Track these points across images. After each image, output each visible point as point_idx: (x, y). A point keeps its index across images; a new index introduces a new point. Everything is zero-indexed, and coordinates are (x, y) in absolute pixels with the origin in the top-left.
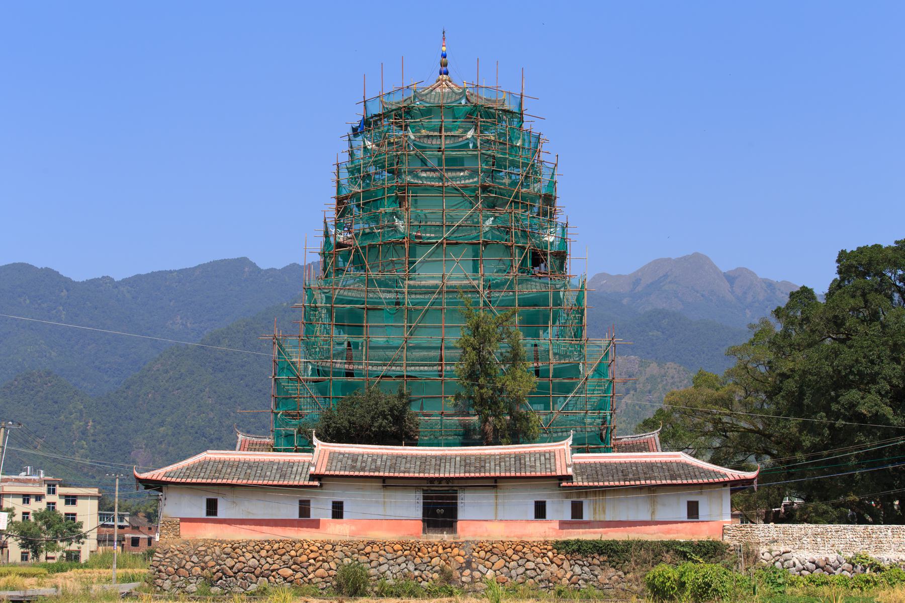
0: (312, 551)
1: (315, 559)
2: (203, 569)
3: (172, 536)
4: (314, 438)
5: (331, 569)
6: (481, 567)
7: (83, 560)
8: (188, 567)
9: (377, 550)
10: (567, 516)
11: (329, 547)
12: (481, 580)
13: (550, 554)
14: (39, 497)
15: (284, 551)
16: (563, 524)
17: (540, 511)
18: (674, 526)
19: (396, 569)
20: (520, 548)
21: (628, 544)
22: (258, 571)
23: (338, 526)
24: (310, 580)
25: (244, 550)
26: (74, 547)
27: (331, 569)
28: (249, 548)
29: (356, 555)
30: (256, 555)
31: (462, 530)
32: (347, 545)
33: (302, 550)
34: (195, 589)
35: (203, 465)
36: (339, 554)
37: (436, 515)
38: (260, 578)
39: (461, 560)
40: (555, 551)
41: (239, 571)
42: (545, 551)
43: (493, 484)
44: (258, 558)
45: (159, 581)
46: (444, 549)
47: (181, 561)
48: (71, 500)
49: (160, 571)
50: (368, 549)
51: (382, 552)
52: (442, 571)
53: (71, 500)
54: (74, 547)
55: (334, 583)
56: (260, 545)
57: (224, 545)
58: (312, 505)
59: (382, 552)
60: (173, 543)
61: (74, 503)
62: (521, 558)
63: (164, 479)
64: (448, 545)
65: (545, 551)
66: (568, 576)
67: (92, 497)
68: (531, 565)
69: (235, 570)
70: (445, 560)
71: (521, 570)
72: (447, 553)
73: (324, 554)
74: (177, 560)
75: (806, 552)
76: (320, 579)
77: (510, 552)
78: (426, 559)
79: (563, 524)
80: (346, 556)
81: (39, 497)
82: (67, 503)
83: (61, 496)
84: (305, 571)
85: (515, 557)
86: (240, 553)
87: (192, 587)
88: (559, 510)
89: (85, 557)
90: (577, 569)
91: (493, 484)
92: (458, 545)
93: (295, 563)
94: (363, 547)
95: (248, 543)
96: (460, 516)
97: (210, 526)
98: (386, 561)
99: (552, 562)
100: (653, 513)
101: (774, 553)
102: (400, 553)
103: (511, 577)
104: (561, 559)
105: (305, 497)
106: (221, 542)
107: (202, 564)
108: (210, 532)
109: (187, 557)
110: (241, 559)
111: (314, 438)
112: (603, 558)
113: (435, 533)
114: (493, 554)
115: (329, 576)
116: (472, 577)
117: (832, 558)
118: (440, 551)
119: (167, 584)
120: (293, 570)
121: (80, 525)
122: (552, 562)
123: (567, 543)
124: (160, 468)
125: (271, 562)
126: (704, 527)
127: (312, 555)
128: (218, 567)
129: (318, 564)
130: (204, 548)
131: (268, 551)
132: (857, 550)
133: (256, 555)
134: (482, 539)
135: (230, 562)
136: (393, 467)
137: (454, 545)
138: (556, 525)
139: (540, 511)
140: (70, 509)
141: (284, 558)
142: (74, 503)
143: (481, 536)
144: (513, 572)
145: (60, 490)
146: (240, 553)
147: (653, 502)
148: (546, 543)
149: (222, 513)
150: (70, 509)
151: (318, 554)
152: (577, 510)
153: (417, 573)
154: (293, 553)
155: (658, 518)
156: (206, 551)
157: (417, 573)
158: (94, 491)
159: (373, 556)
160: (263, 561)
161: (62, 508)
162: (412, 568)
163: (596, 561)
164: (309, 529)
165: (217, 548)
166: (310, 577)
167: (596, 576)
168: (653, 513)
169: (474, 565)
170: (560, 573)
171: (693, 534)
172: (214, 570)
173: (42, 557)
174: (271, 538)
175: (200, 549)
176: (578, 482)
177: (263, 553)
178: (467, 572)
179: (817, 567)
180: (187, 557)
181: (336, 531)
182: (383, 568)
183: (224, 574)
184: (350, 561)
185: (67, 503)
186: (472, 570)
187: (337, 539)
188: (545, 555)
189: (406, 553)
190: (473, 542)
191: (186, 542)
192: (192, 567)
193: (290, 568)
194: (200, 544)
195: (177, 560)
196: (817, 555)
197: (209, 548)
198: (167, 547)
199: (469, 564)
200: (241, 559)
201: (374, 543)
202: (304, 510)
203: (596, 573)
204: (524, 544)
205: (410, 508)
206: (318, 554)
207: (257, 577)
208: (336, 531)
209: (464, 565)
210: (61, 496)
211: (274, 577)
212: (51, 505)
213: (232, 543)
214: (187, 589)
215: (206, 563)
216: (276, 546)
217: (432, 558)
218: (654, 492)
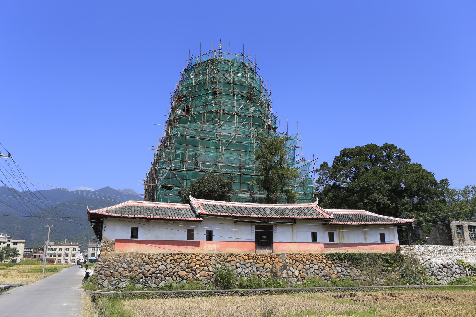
0: (197, 260)
1: (199, 265)
2: (130, 272)
3: (109, 250)
4: (190, 196)
5: (209, 271)
6: (291, 269)
7: (17, 262)
8: (120, 271)
9: (235, 259)
10: (327, 241)
11: (207, 257)
12: (293, 277)
13: (324, 261)
14: (4, 243)
15: (181, 260)
16: (326, 245)
17: (314, 238)
18: (375, 246)
19: (247, 271)
20: (310, 258)
21: (361, 255)
22: (165, 273)
23: (209, 245)
24: (197, 278)
25: (156, 259)
26: (15, 258)
27: (209, 271)
28: (159, 258)
29: (223, 262)
30: (164, 263)
31: (276, 248)
32: (218, 256)
33: (191, 260)
34: (125, 286)
35: (128, 208)
36: (214, 262)
37: (262, 239)
38: (167, 278)
39: (281, 265)
40: (327, 259)
41: (153, 273)
42: (322, 259)
43: (292, 222)
44: (165, 264)
45: (101, 281)
46: (271, 258)
47: (115, 267)
48: (15, 243)
49: (101, 274)
50: (230, 259)
51: (238, 260)
52: (272, 271)
53: (15, 243)
54: (15, 258)
55: (212, 280)
56: (166, 256)
57: (144, 256)
58: (195, 232)
59: (238, 260)
60: (110, 255)
61: (16, 244)
62: (311, 263)
63: (107, 214)
64: (273, 256)
65: (322, 259)
66: (336, 272)
67: (23, 243)
68: (316, 267)
69: (150, 272)
70: (272, 265)
71: (312, 270)
72: (273, 261)
73: (205, 262)
74: (112, 266)
75: (437, 259)
76: (203, 278)
77: (305, 260)
78: (262, 265)
79: (326, 245)
80: (218, 263)
81: (4, 243)
82: (14, 244)
83: (12, 242)
84: (194, 272)
85: (308, 263)
86: (154, 261)
87: (123, 285)
88: (323, 237)
89: (18, 261)
90: (339, 269)
91: (292, 222)
92: (278, 256)
93: (188, 268)
94: (227, 257)
95: (159, 255)
96: (275, 240)
97: (133, 244)
98: (240, 266)
99: (326, 265)
100: (365, 239)
101: (425, 260)
102: (247, 261)
103: (307, 274)
104: (331, 264)
105: (191, 227)
106: (142, 254)
107: (130, 269)
108: (133, 248)
109: (119, 264)
110: (155, 265)
111: (190, 196)
112: (350, 263)
113: (261, 249)
114: (296, 261)
115: (209, 275)
116: (288, 275)
117: (450, 262)
118: (269, 260)
119: (106, 283)
120: (187, 272)
121: (18, 251)
122: (326, 265)
123: (332, 255)
124: (104, 207)
125: (174, 267)
126: (388, 246)
127: (198, 263)
128: (140, 271)
129: (202, 268)
130: (131, 259)
131: (171, 260)
132: (458, 258)
133: (164, 263)
134: (290, 253)
135: (147, 267)
136: (239, 212)
137: (276, 256)
138: (322, 245)
139: (314, 238)
140: (15, 246)
141: (181, 264)
142: (16, 244)
143: (286, 251)
144: (308, 271)
145: (12, 240)
146: (154, 261)
147: (365, 234)
148: (322, 255)
149: (141, 236)
150: (15, 246)
151: (201, 262)
152: (331, 237)
153: (258, 273)
154: (186, 261)
155: (368, 241)
156: (132, 260)
157: (258, 273)
158: (24, 241)
159: (233, 263)
160: (168, 266)
161: (12, 246)
162: (255, 270)
163: (347, 265)
164: (193, 247)
165: (139, 258)
166: (198, 276)
167: (349, 273)
168: (365, 239)
169: (288, 268)
170: (331, 271)
171: (384, 250)
172: (138, 273)
173: (3, 262)
174: (172, 252)
175: (128, 259)
176: (335, 222)
177: (168, 261)
178: (285, 272)
179: (444, 267)
180: (119, 264)
181: (208, 248)
182: (240, 270)
183: (144, 275)
184: (220, 266)
185: (14, 244)
186: (287, 270)
187: (212, 253)
188: (322, 262)
189: (251, 261)
190: (286, 254)
191: (119, 255)
192: (123, 271)
193: (185, 270)
194: (128, 256)
195: (112, 266)
196: (442, 261)
197: (134, 258)
198: (106, 257)
199: (285, 267)
200: (155, 265)
201: (232, 255)
202: (190, 235)
203: (348, 271)
204: (311, 255)
205: (248, 234)
206: (201, 262)
207: (165, 277)
208: (208, 248)
209: (283, 267)
210: (12, 242)
211: (175, 276)
212: (8, 245)
213: (149, 255)
214: (119, 286)
215: (132, 268)
216: (176, 257)
217: (265, 264)
218: (365, 228)
